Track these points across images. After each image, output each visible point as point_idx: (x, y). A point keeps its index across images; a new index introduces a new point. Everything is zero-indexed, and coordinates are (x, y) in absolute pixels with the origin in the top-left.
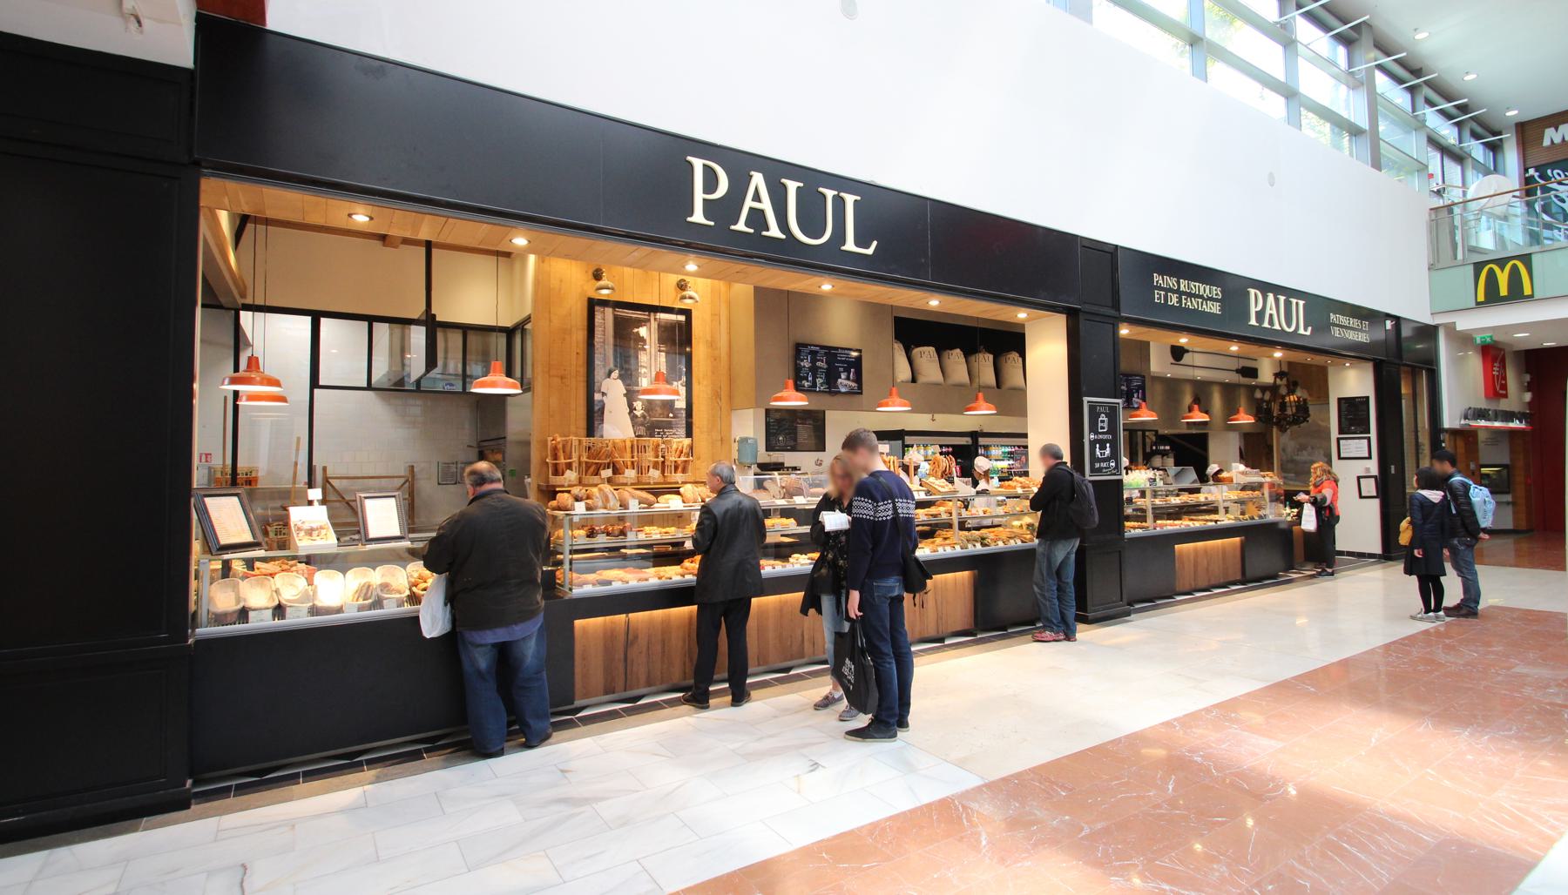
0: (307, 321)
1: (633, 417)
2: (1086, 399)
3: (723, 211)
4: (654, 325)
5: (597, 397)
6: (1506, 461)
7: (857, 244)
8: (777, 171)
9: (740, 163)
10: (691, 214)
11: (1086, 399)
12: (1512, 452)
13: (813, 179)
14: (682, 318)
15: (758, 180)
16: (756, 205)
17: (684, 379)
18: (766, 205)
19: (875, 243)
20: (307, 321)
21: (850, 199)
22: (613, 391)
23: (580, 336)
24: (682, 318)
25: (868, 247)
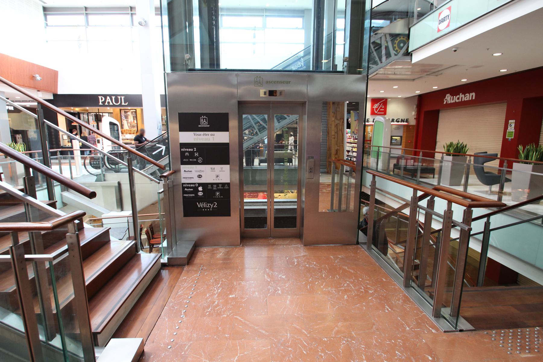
0: (441, 154)
1: (128, 126)
2: (507, 138)
3: (104, 102)
4: (130, 112)
5: (123, 123)
6: (402, 135)
7: (124, 103)
8: (110, 96)
9: (105, 96)
10: (115, 98)
11: (507, 138)
12: (404, 132)
13: (116, 96)
14: (135, 110)
15: (108, 98)
16: (109, 101)
17: (136, 120)
18: (110, 101)
19: (127, 103)
20: (378, 147)
21: (123, 97)
22: (125, 122)
23: (119, 114)
24: (135, 110)
25: (126, 103)
